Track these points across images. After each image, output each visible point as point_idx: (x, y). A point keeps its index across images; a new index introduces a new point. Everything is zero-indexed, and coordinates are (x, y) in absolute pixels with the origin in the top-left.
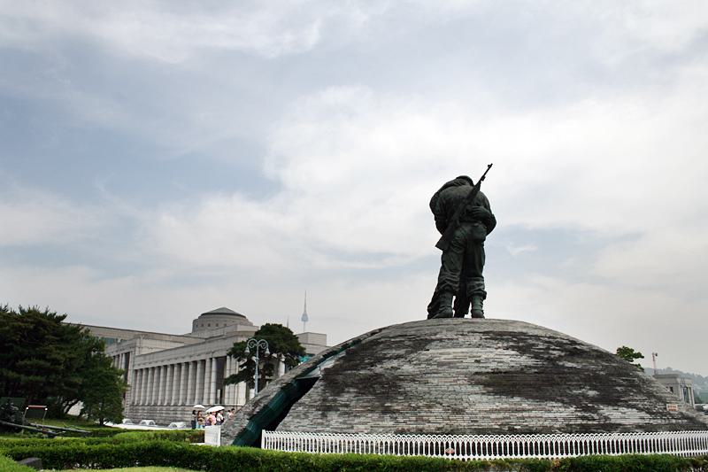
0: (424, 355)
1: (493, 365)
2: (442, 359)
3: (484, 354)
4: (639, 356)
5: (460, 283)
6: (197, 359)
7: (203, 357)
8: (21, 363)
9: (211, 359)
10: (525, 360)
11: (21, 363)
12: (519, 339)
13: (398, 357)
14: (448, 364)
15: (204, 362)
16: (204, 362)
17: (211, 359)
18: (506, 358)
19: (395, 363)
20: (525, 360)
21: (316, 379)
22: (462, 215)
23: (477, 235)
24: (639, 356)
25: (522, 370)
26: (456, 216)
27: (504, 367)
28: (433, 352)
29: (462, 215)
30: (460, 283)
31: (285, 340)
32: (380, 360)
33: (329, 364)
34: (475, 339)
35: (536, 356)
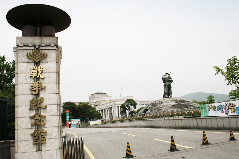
0: (163, 104)
1: (172, 105)
2: (165, 104)
3: (170, 103)
4: (213, 97)
5: (168, 92)
6: (103, 109)
7: (104, 108)
8: (84, 114)
9: (107, 108)
10: (176, 104)
11: (84, 114)
12: (176, 101)
13: (159, 105)
14: (166, 105)
15: (105, 109)
16: (105, 109)
17: (107, 108)
18: (174, 103)
19: (159, 106)
20: (176, 104)
21: (148, 109)
22: (167, 81)
23: (170, 84)
24: (213, 97)
25: (175, 105)
26: (166, 81)
27: (173, 105)
28: (164, 104)
29: (167, 81)
30: (168, 92)
31: (133, 102)
32: (157, 105)
33: (150, 107)
34: (169, 101)
35: (178, 103)
